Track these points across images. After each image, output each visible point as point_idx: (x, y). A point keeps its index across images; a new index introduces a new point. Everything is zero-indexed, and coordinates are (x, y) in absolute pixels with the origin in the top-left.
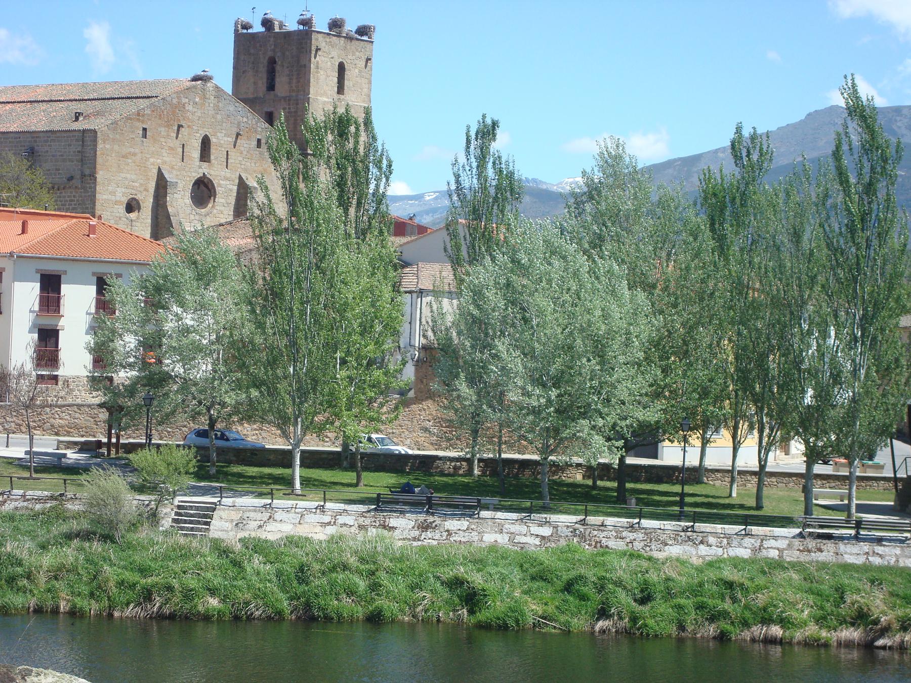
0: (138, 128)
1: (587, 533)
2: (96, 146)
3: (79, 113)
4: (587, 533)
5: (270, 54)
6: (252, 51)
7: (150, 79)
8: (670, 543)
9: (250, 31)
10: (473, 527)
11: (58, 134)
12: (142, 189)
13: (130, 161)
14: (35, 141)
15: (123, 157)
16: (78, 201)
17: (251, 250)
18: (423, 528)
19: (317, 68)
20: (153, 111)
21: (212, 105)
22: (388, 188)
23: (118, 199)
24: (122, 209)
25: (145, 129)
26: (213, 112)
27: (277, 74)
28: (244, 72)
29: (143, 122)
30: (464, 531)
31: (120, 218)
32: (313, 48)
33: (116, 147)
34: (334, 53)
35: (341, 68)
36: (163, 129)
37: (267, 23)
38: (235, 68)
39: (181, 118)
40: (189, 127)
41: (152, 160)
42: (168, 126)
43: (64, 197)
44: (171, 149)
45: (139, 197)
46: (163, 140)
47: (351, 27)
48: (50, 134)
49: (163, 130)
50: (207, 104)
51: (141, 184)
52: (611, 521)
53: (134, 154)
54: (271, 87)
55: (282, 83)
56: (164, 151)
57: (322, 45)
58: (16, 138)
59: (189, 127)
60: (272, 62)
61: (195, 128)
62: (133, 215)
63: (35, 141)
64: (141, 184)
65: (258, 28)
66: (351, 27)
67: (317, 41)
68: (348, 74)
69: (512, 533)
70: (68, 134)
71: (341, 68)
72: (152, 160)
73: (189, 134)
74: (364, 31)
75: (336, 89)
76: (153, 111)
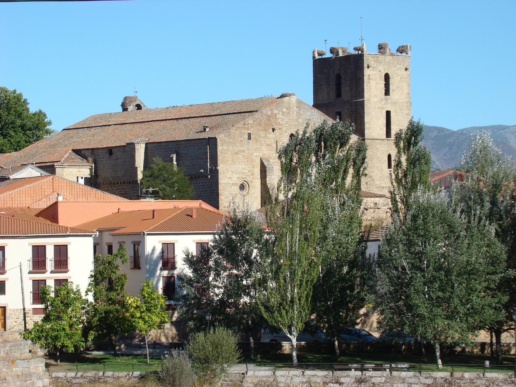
0: (244, 134)
1: (453, 381)
2: (217, 148)
3: (207, 127)
4: (453, 381)
5: (337, 72)
6: (325, 71)
7: (254, 97)
8: (501, 385)
9: (323, 57)
10: (388, 380)
11: (193, 142)
12: (250, 174)
13: (240, 156)
14: (179, 147)
15: (236, 154)
16: (208, 185)
17: (383, 187)
18: (359, 382)
19: (369, 79)
20: (254, 121)
21: (295, 113)
22: (363, 179)
23: (234, 182)
24: (237, 188)
25: (249, 135)
26: (296, 118)
27: (342, 86)
28: (320, 86)
29: (248, 129)
30: (383, 383)
31: (236, 195)
32: (365, 65)
33: (231, 148)
34: (381, 68)
35: (387, 77)
36: (262, 133)
37: (333, 50)
38: (314, 83)
39: (274, 124)
40: (280, 129)
41: (255, 154)
42: (265, 130)
43: (199, 183)
44: (268, 145)
45: (248, 179)
46: (262, 140)
47: (393, 47)
48: (188, 142)
49: (262, 133)
50: (292, 113)
51: (249, 171)
52: (467, 375)
53: (243, 151)
54: (339, 95)
55: (345, 90)
56: (263, 147)
57: (372, 63)
58: (166, 146)
59: (280, 129)
60: (339, 77)
61: (284, 129)
62: (245, 192)
63: (179, 147)
64: (249, 171)
65: (328, 55)
66: (393, 47)
67: (367, 60)
68: (391, 81)
69: (409, 383)
70: (199, 141)
71: (387, 77)
72: (255, 154)
73: (280, 134)
74: (402, 50)
75: (384, 92)
76: (254, 121)
